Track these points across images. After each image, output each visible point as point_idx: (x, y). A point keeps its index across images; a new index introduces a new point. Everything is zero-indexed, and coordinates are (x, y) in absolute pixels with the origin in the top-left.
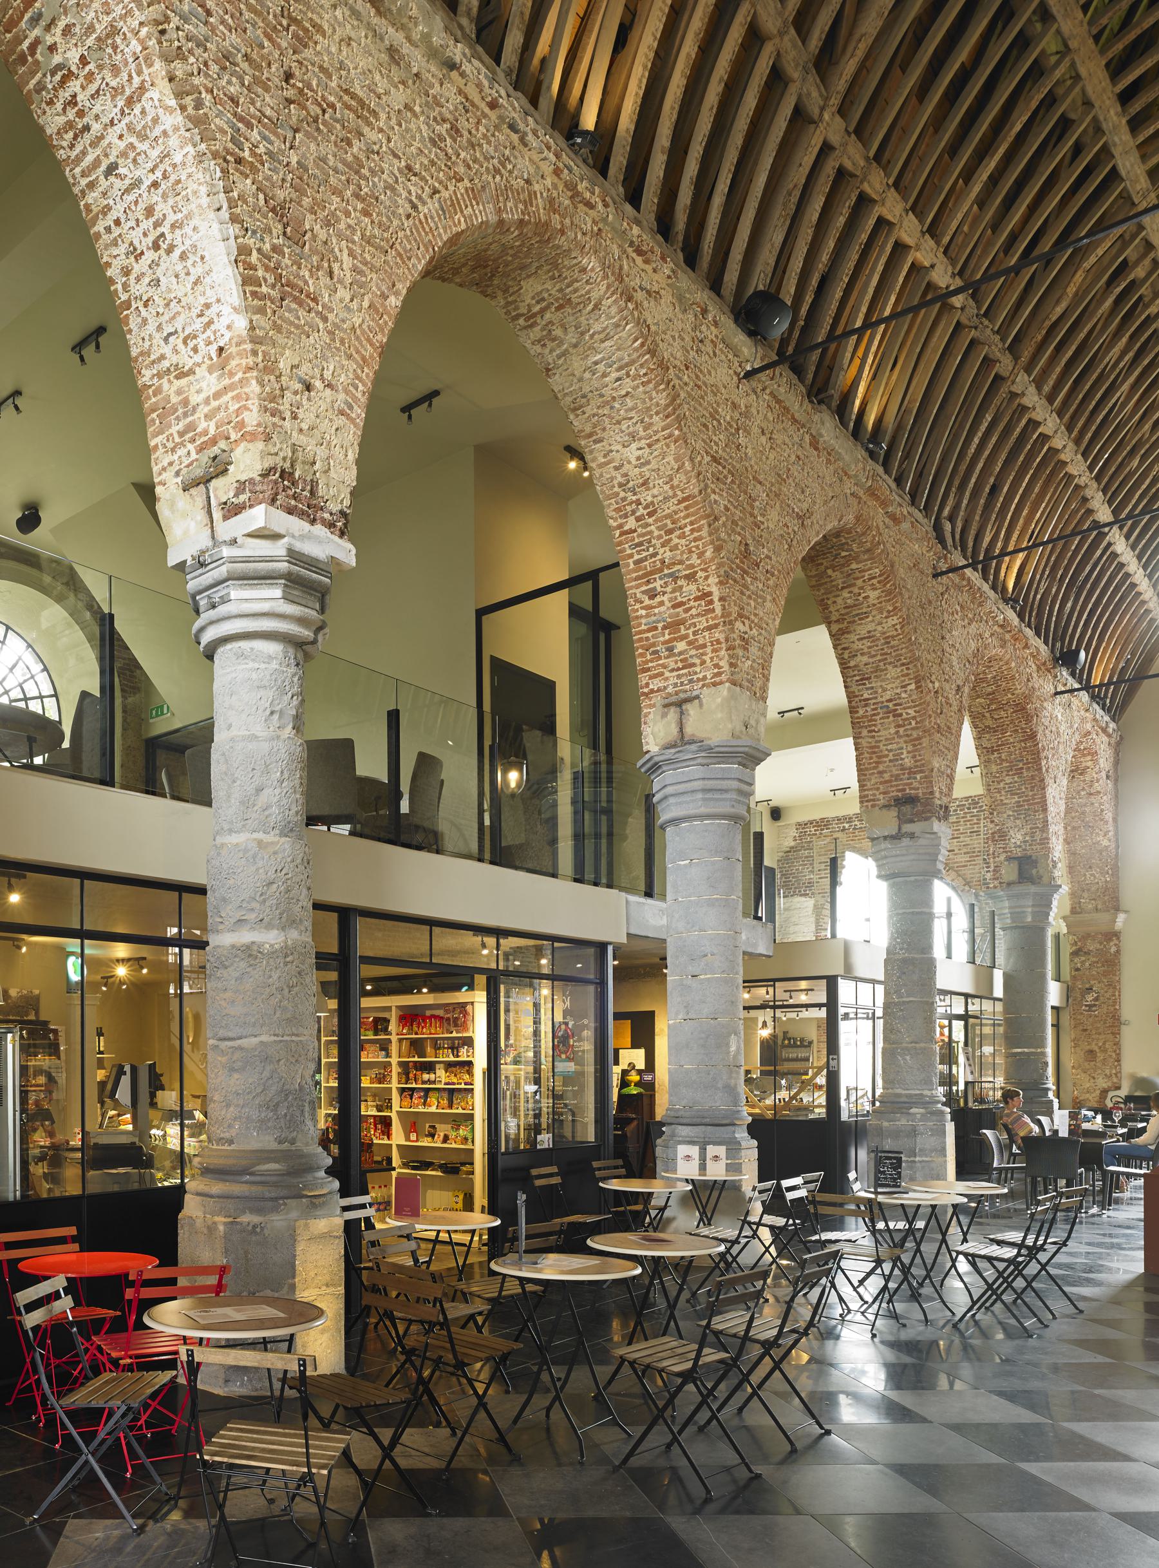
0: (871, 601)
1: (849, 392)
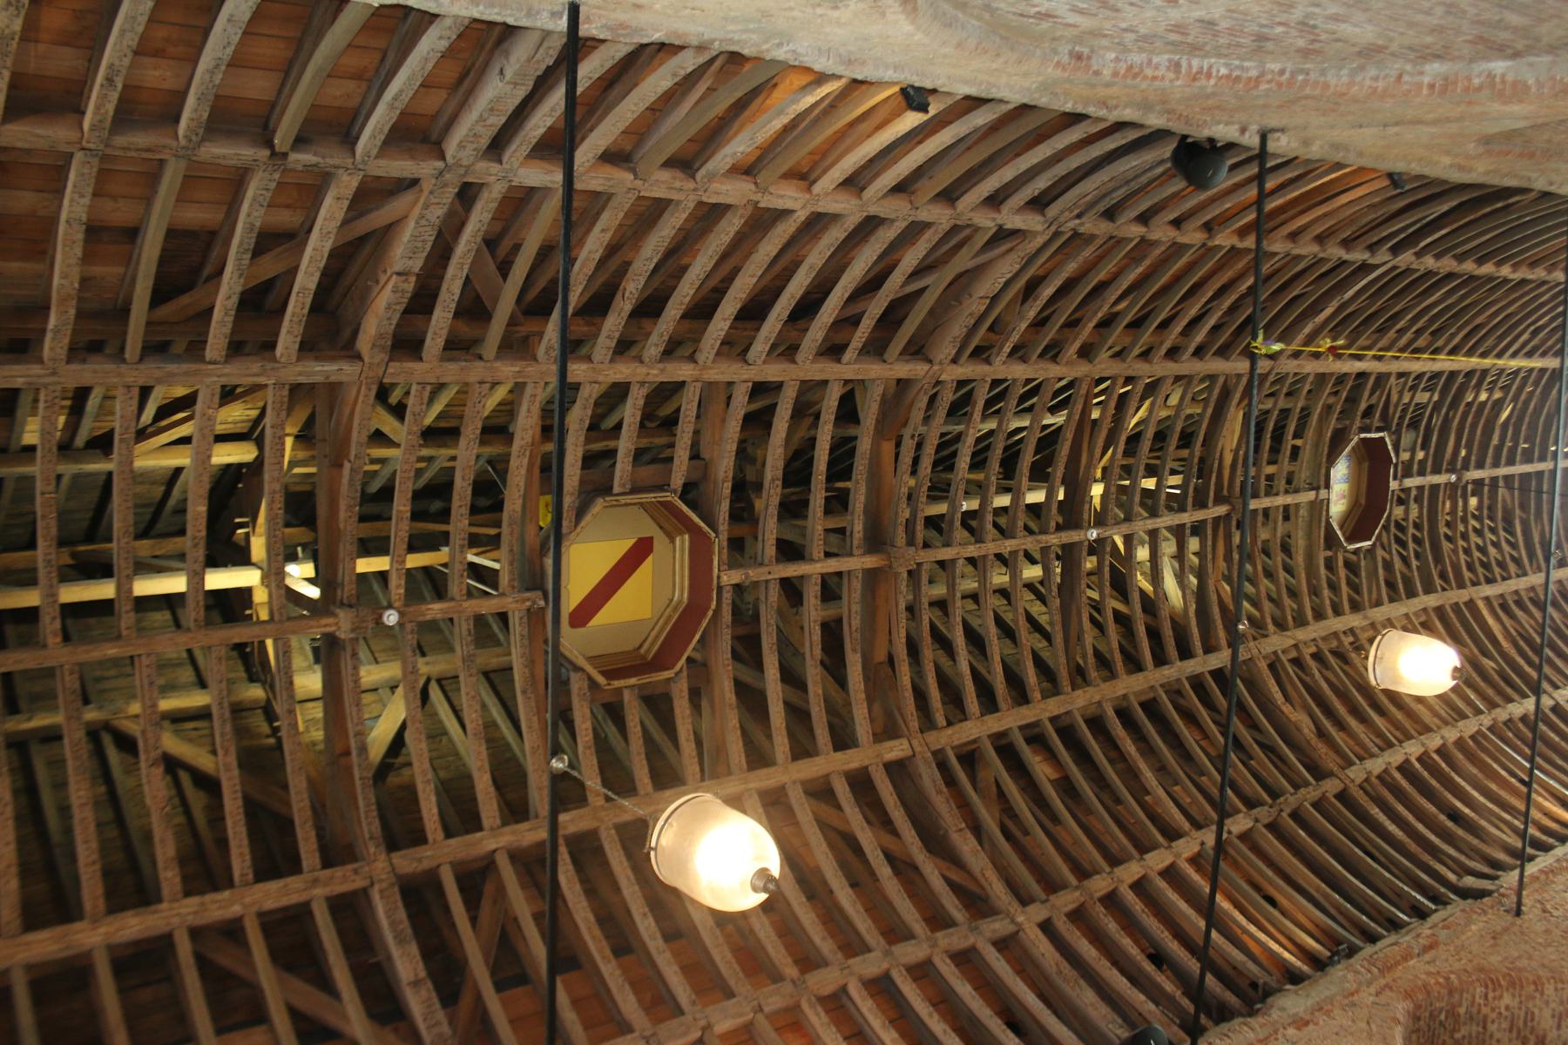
0: (1514, 1003)
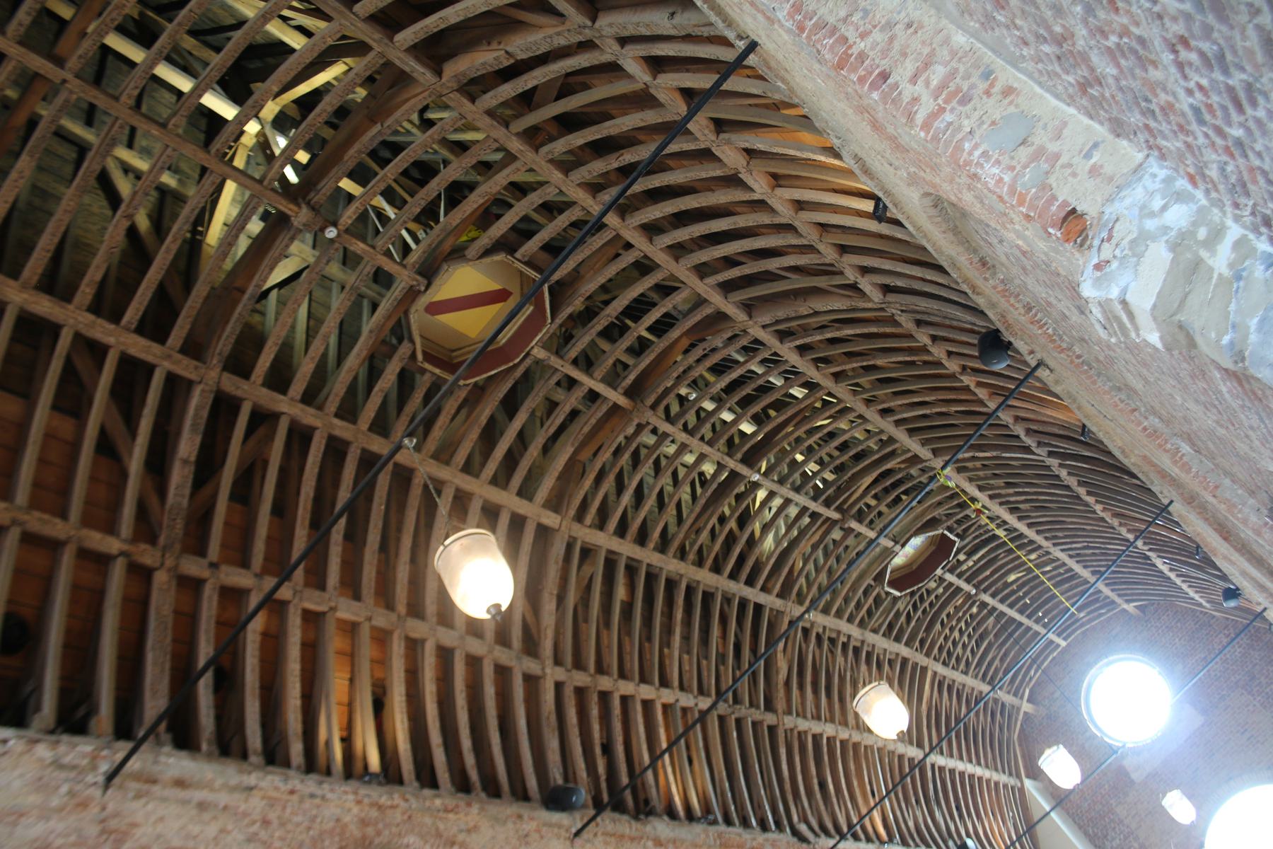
1: (534, 26)
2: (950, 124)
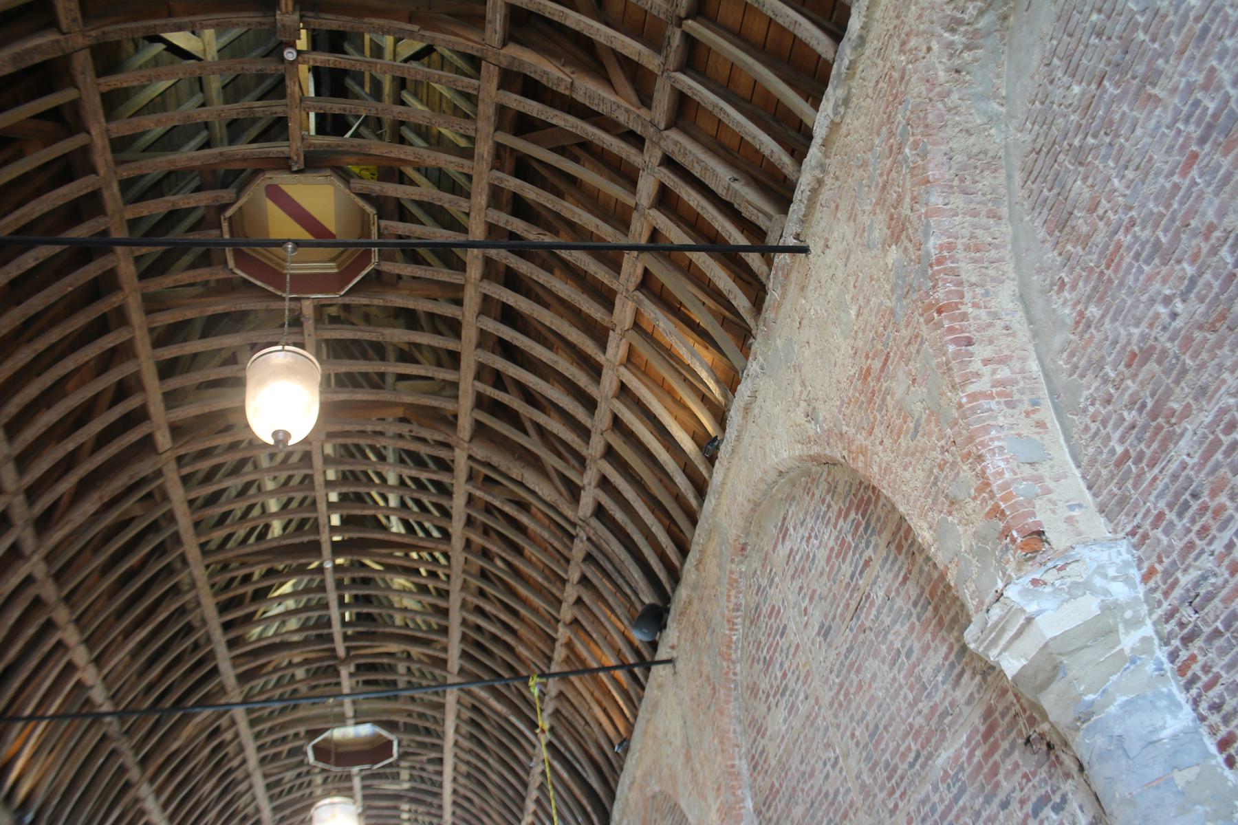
2: (990, 410)
